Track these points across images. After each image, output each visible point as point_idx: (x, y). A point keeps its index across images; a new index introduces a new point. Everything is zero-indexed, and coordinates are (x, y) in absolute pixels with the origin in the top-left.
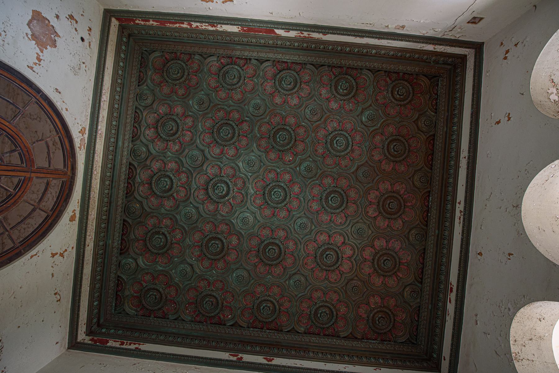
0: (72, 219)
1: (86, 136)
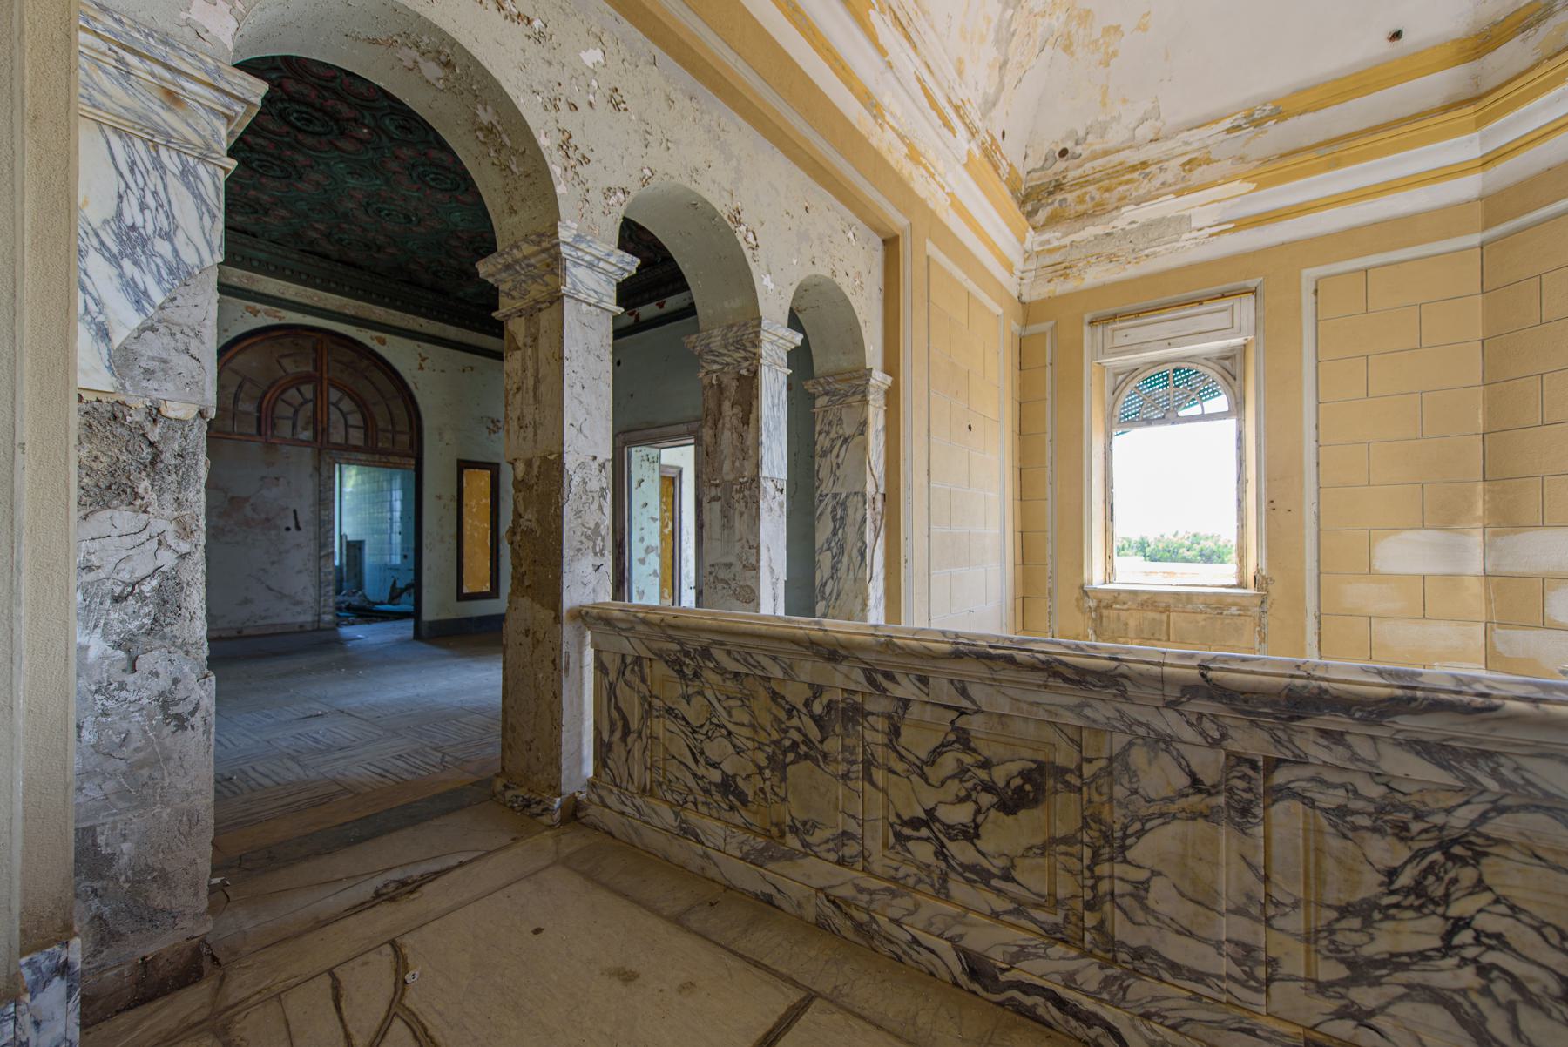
0: (383, 342)
1: (259, 306)
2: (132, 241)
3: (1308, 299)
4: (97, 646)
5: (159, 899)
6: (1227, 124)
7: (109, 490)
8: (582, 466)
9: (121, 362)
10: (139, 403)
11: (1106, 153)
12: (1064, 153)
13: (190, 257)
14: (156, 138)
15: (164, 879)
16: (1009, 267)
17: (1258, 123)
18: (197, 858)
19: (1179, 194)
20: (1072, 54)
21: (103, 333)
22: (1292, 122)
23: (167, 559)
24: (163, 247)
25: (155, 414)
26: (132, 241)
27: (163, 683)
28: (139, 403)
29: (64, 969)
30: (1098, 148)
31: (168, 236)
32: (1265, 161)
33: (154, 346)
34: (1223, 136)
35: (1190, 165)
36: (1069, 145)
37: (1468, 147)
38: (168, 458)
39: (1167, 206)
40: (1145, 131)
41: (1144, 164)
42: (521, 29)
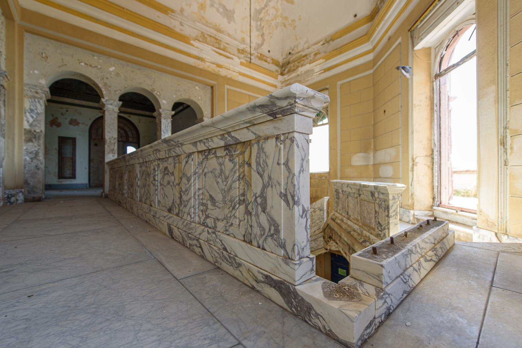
0: (130, 117)
2: (32, 111)
3: (338, 91)
4: (28, 158)
5: (35, 190)
6: (321, 43)
7: (29, 140)
8: (110, 138)
9: (31, 125)
10: (33, 130)
11: (298, 52)
12: (290, 53)
13: (39, 112)
14: (35, 97)
15: (36, 188)
16: (275, 86)
17: (328, 42)
18: (41, 186)
19: (310, 64)
20: (286, 27)
21: (28, 122)
22: (336, 41)
23: (36, 149)
24: (36, 111)
25: (35, 131)
26: (32, 111)
27: (36, 164)
28: (33, 130)
29: (22, 192)
30: (297, 51)
31: (36, 109)
32: (330, 52)
33: (35, 123)
34: (321, 46)
35: (316, 55)
36: (291, 51)
37: (367, 47)
38: (37, 137)
39: (308, 67)
40: (306, 46)
41: (306, 55)
42: (95, 69)
